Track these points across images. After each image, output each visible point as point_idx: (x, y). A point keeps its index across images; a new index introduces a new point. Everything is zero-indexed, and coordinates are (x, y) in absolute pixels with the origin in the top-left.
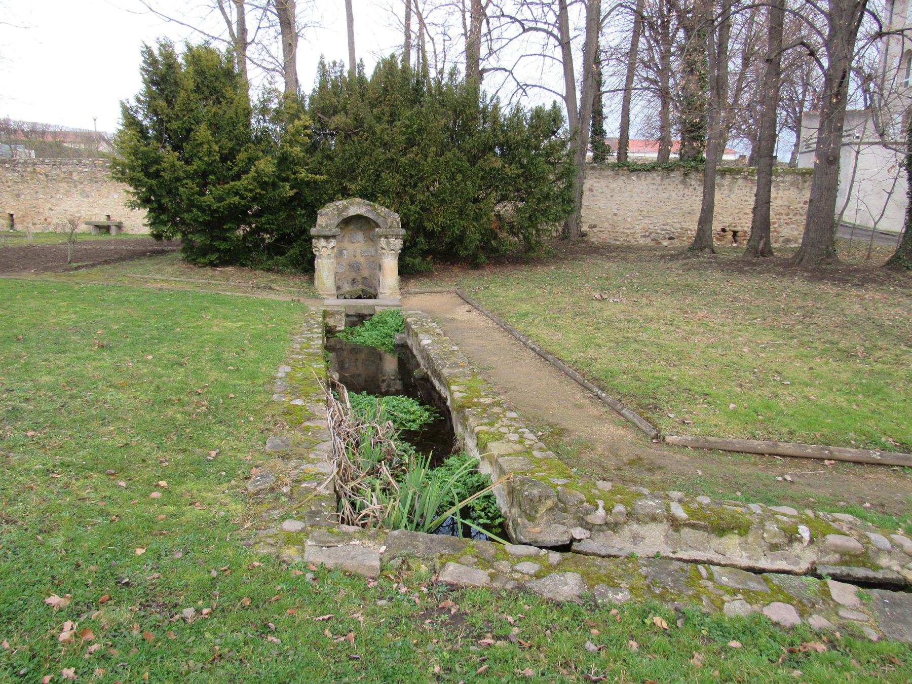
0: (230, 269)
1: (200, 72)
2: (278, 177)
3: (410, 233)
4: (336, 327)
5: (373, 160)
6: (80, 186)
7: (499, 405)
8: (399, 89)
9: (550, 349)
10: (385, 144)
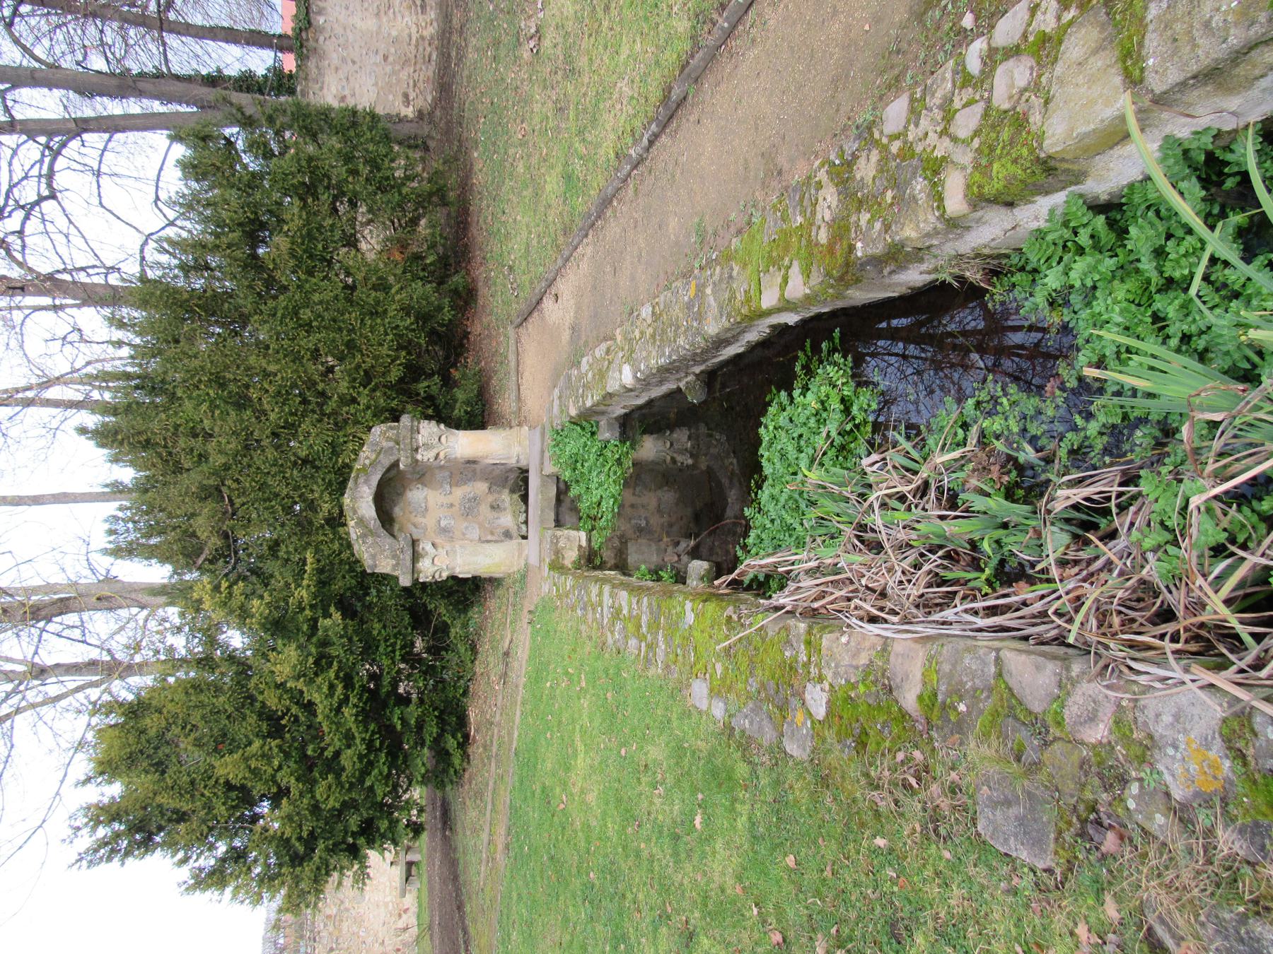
0: (473, 715)
1: (131, 760)
2: (309, 638)
3: (409, 407)
4: (580, 547)
5: (274, 470)
6: (347, 904)
7: (849, 164)
8: (139, 422)
9: (655, 95)
10: (247, 447)
